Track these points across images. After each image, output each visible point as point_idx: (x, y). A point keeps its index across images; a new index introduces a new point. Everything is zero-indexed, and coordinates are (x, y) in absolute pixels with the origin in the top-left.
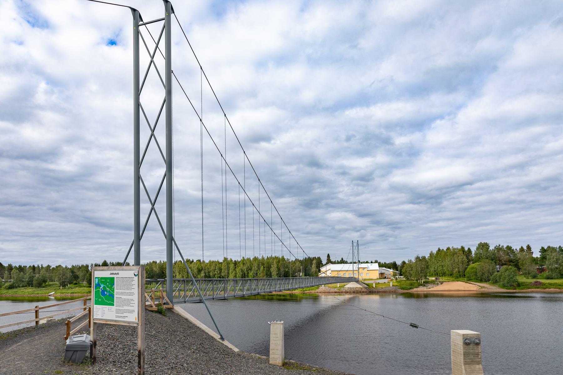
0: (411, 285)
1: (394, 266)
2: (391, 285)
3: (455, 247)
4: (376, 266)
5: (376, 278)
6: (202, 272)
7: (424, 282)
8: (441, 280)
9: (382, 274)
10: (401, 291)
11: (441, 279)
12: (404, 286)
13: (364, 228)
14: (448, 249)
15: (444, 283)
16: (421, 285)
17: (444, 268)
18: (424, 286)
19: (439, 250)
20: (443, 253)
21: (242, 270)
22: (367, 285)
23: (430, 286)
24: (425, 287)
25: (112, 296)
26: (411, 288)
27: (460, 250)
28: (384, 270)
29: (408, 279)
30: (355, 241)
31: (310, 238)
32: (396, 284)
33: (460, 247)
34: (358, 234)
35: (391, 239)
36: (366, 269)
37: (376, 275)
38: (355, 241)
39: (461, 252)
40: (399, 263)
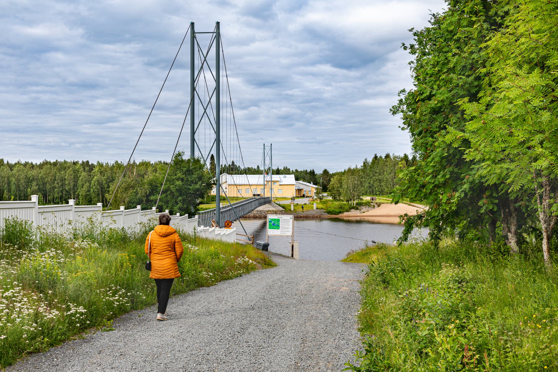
0: (341, 208)
1: (309, 176)
2: (315, 208)
3: (397, 154)
4: (291, 179)
5: (291, 196)
6: (34, 183)
7: (357, 204)
8: (378, 201)
9: (299, 190)
10: (327, 216)
11: (379, 199)
12: (331, 209)
13: (255, 103)
14: (387, 156)
15: (382, 205)
16: (353, 208)
17: (383, 184)
18: (357, 209)
19: (376, 157)
20: (381, 163)
21: (98, 181)
22: (283, 207)
23: (364, 209)
24: (358, 211)
25: (279, 226)
26: (340, 212)
27: (402, 159)
28: (302, 184)
29: (335, 198)
30: (268, 144)
31: (161, 116)
32: (321, 206)
33: (402, 155)
34: (245, 112)
35: (299, 125)
36: (278, 184)
37: (292, 193)
38: (268, 144)
39: (404, 162)
40: (319, 171)
